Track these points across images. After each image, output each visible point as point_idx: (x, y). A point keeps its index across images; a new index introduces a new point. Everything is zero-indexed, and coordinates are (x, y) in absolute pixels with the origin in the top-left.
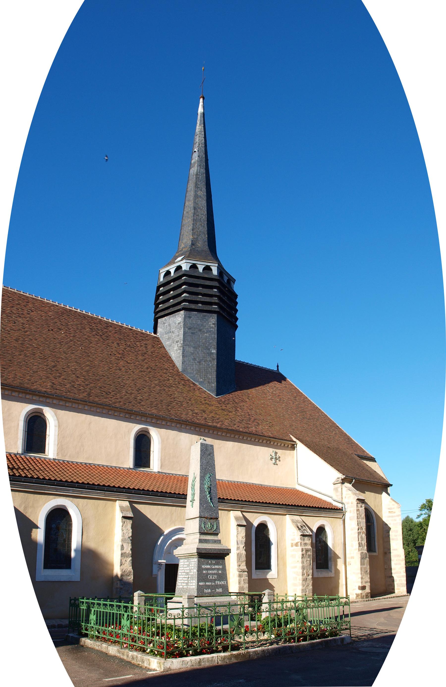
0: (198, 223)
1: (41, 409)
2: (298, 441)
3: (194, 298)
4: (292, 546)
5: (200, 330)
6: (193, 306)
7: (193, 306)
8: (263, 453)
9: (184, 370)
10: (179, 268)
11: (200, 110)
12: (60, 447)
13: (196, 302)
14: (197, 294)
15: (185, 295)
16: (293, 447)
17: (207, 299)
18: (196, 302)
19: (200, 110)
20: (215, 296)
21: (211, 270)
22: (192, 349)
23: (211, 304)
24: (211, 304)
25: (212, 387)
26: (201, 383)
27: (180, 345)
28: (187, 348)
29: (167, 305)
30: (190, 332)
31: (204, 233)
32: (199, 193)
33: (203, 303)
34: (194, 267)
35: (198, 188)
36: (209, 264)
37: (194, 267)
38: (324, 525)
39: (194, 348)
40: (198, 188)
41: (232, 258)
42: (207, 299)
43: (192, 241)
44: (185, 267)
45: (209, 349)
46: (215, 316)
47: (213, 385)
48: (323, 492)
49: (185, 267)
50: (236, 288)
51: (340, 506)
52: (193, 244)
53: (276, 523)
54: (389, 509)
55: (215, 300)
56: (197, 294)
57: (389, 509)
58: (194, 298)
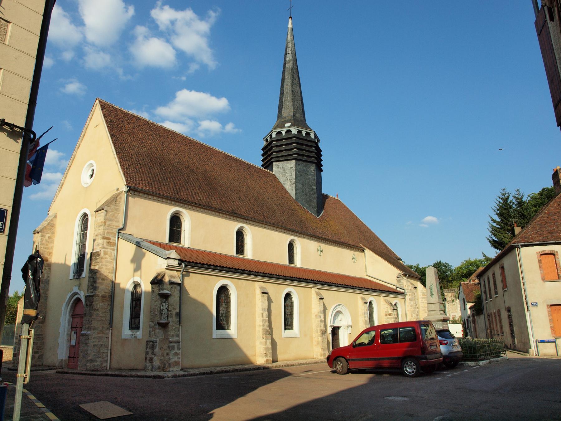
0: (296, 102)
1: (179, 211)
2: (365, 248)
3: (300, 152)
5: (306, 174)
6: (301, 158)
8: (347, 253)
9: (297, 198)
10: (289, 131)
11: (290, 26)
12: (254, 252)
13: (302, 155)
14: (302, 150)
15: (295, 150)
16: (363, 251)
17: (309, 154)
18: (302, 155)
20: (314, 152)
23: (312, 157)
27: (293, 182)
28: (298, 185)
33: (306, 156)
34: (300, 132)
38: (227, 285)
41: (317, 124)
42: (309, 154)
44: (294, 131)
46: (315, 165)
49: (294, 131)
51: (403, 291)
52: (294, 115)
53: (238, 288)
55: (314, 155)
56: (302, 150)
58: (300, 152)
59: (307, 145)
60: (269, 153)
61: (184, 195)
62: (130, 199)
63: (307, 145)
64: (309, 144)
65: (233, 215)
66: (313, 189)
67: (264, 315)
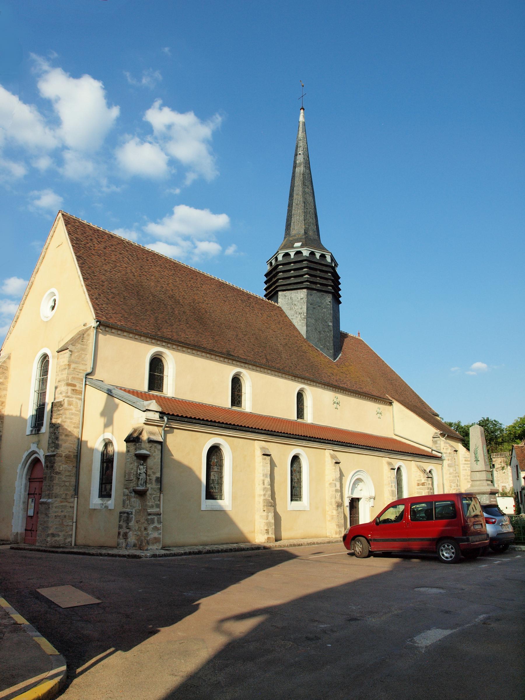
0: (308, 216)
2: (393, 400)
4: (418, 485)
5: (319, 306)
6: (314, 286)
7: (314, 286)
9: (308, 337)
10: (299, 253)
11: (301, 119)
13: (315, 283)
15: (307, 276)
16: (391, 404)
17: (324, 282)
18: (315, 283)
19: (301, 119)
20: (330, 279)
21: (290, 255)
22: (314, 321)
23: (327, 285)
24: (327, 285)
25: (331, 353)
26: (321, 349)
27: (303, 317)
28: (310, 320)
29: (288, 282)
30: (311, 306)
31: (313, 224)
32: (306, 190)
33: (321, 284)
34: (312, 254)
35: (306, 185)
36: (324, 253)
37: (287, 255)
39: (315, 320)
40: (306, 185)
42: (324, 282)
43: (305, 230)
44: (306, 253)
45: (326, 322)
47: (331, 351)
48: (421, 443)
49: (306, 253)
50: (338, 270)
51: (439, 455)
53: (233, 449)
54: (465, 458)
57: (465, 458)
59: (321, 271)
60: (274, 280)
61: (167, 332)
62: (101, 336)
63: (321, 271)
64: (324, 268)
65: (228, 357)
66: (329, 326)
67: (266, 482)
